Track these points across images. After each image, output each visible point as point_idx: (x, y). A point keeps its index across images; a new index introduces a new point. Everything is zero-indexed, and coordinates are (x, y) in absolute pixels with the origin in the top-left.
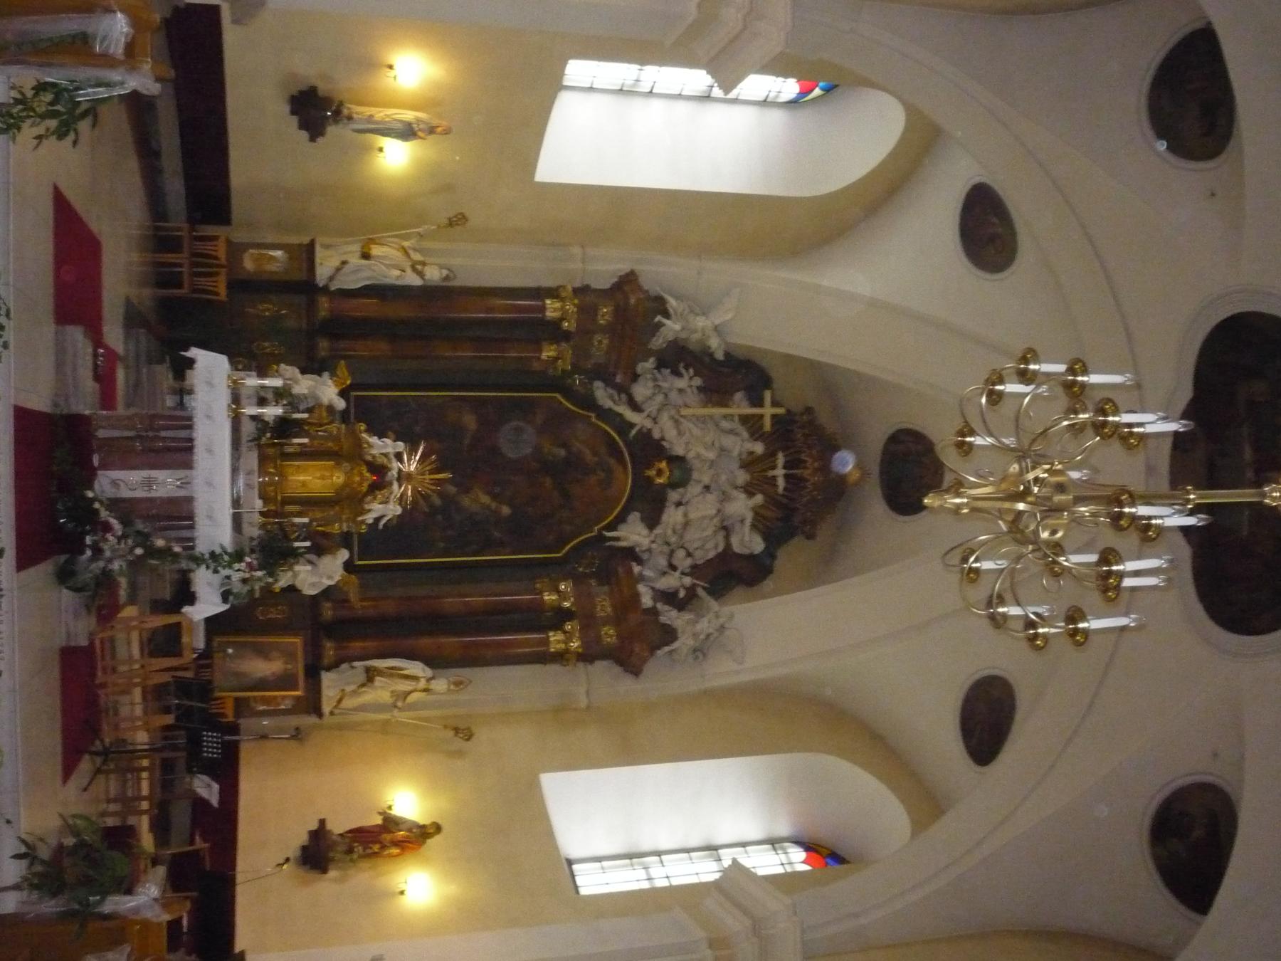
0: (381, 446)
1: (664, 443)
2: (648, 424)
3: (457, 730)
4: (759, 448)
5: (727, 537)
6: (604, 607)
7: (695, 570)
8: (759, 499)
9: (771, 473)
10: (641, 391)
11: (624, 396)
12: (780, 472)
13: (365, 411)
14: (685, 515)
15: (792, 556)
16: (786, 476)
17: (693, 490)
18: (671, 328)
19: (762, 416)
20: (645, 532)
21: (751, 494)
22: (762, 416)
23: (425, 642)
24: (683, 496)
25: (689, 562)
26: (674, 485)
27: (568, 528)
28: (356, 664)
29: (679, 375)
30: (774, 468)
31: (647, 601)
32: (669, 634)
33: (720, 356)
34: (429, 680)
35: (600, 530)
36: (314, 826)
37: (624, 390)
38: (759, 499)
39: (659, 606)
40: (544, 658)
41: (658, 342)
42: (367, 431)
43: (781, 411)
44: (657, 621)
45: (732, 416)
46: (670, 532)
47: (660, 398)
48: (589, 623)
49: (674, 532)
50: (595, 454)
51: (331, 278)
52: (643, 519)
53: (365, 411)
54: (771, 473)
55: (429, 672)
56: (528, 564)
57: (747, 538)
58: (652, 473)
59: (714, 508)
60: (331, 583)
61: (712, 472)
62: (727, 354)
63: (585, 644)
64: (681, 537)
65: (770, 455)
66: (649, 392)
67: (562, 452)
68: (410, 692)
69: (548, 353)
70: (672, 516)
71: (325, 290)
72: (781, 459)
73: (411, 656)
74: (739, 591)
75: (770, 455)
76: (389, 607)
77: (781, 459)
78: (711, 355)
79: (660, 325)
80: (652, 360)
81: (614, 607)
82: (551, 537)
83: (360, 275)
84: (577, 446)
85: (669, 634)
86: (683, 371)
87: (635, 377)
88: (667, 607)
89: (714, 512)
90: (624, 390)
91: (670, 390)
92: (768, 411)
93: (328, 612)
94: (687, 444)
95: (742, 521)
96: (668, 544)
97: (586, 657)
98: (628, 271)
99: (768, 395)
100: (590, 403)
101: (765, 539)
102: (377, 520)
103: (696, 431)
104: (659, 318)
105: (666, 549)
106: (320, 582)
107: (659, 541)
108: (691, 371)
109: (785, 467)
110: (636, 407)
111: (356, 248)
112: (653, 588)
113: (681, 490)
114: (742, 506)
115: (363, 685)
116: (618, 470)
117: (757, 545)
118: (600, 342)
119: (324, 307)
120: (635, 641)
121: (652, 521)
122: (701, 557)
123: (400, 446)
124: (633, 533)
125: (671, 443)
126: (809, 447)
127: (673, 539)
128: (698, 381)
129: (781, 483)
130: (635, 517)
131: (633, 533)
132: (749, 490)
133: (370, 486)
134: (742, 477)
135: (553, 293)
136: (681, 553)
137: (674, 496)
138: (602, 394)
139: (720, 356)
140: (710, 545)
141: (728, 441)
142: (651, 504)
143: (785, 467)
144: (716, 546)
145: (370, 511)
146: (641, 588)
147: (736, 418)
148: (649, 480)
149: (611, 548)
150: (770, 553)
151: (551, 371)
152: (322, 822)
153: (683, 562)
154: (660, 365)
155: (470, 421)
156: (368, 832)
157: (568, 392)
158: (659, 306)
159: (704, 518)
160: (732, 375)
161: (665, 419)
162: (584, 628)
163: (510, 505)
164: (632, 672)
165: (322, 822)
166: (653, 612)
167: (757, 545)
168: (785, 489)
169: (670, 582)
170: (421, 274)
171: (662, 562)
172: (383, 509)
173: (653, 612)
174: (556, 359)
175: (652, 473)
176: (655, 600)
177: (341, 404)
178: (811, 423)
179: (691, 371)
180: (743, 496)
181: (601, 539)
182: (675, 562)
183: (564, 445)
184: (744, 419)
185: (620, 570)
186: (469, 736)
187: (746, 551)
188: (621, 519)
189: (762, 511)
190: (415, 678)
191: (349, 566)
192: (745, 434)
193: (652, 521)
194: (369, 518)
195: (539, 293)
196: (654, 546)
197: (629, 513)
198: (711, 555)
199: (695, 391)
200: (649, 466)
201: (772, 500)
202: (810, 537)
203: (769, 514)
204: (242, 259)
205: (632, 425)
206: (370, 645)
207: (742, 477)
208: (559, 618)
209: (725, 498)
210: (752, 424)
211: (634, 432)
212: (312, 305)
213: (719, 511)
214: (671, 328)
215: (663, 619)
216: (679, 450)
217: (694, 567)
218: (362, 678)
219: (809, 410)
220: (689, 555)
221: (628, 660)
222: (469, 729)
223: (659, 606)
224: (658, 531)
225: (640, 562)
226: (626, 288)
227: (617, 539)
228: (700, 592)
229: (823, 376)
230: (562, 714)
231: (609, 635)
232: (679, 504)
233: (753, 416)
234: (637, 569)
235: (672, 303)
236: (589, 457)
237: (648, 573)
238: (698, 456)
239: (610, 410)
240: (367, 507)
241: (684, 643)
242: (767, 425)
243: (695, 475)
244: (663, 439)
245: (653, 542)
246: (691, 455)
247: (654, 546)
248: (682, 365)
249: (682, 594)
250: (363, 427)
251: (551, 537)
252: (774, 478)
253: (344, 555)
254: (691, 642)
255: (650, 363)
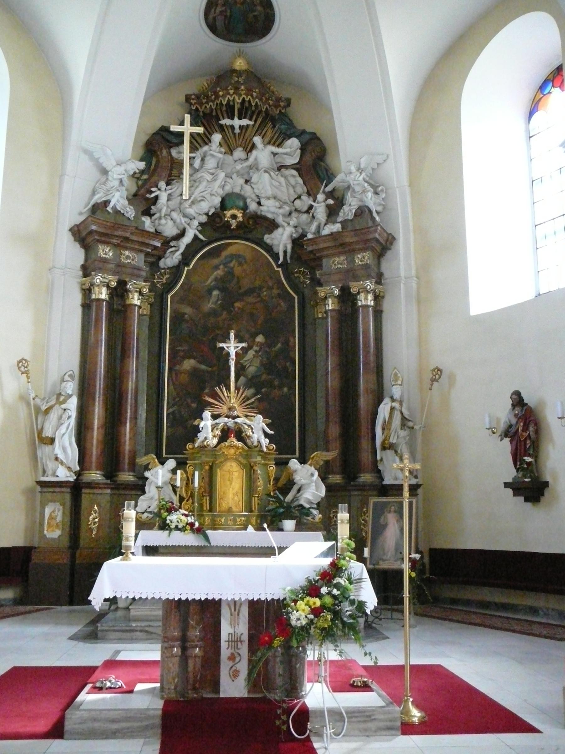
0: (208, 428)
1: (210, 214)
2: (196, 223)
3: (433, 380)
4: (217, 137)
5: (286, 167)
6: (338, 262)
7: (312, 194)
8: (257, 140)
9: (237, 131)
10: (169, 229)
11: (172, 244)
12: (237, 123)
13: (177, 442)
14: (268, 198)
15: (304, 119)
16: (240, 118)
17: (248, 191)
18: (119, 200)
19: (191, 135)
20: (280, 230)
21: (254, 146)
22: (191, 135)
23: (363, 402)
24: (253, 200)
25: (305, 197)
26: (245, 208)
27: (275, 291)
28: (379, 458)
29: (157, 198)
30: (232, 127)
31: (336, 227)
32: (363, 212)
33: (142, 165)
34: (393, 400)
35: (278, 266)
36: (510, 491)
37: (167, 243)
38: (257, 140)
39: (340, 219)
40: (378, 313)
41: (130, 212)
42: (193, 441)
43: (187, 117)
44: (351, 220)
45: (190, 158)
46: (281, 211)
47: (175, 215)
48: (352, 274)
49: (280, 208)
50: (217, 268)
51: (69, 468)
52: (271, 232)
53: (177, 442)
54: (237, 131)
55: (387, 400)
56: (302, 325)
57: (288, 150)
58: (234, 224)
59: (266, 177)
60: (316, 473)
61: (234, 176)
62: (141, 160)
63: (369, 277)
64: (285, 203)
65: (222, 129)
66: (170, 223)
67: (215, 293)
68: (402, 413)
69: (135, 299)
70: (269, 208)
71: (79, 474)
72: (226, 122)
73: (374, 414)
74: (330, 160)
75: (222, 129)
76: (335, 431)
77: (226, 122)
78: (142, 172)
79: (114, 208)
80: (143, 219)
81: (340, 254)
82: (282, 304)
83: (67, 444)
84: (210, 281)
85: (363, 212)
86: (153, 195)
87: (157, 234)
88: (341, 214)
89: (266, 175)
90: (167, 243)
91: (168, 207)
92: (188, 129)
93: (336, 479)
94: (212, 195)
95: (275, 154)
96: (290, 214)
97: (379, 279)
98: (70, 234)
99: (175, 128)
100: (176, 271)
101: (290, 137)
102: (266, 435)
103: (201, 188)
104: (109, 209)
105: (294, 215)
106: (315, 482)
107: (287, 220)
108: (153, 189)
109: (233, 119)
110: (182, 234)
111: (47, 449)
112: (325, 224)
113: (248, 201)
114: (263, 154)
115: (396, 452)
116: (230, 250)
117: (293, 143)
118: (128, 257)
119: (95, 476)
120: (368, 238)
121: (272, 225)
122: (301, 188)
123: (207, 414)
124: (281, 239)
125: (211, 207)
126: (217, 97)
127: (287, 209)
128: (162, 184)
129: (245, 122)
130: (267, 238)
131: (281, 239)
132: (250, 148)
133: (238, 441)
134: (239, 153)
135: (87, 292)
136: (298, 203)
137: (253, 206)
138: (172, 259)
139: (142, 165)
140: (292, 181)
141: (211, 163)
142: (257, 226)
143: (233, 119)
144: (293, 176)
145: (259, 442)
146: (326, 231)
147: (193, 155)
148: (240, 226)
149: (291, 258)
150: (300, 134)
151: (152, 300)
152: (507, 485)
153: (307, 201)
154: (148, 213)
155: (188, 364)
156: (516, 449)
157: (169, 286)
158: (99, 208)
159: (271, 184)
160: (158, 151)
161: (191, 211)
162: (356, 278)
163: (257, 334)
164: (391, 243)
165: (507, 485)
166: (344, 223)
167: (293, 143)
168: (250, 120)
169: (320, 211)
170: (70, 396)
171: (304, 217)
172: (257, 428)
173: (344, 223)
174: (140, 293)
175: (234, 224)
176: (334, 222)
177: (171, 463)
178: (198, 97)
179: (153, 189)
180: (254, 153)
181: (284, 265)
182: (305, 209)
183: (210, 291)
184: (193, 148)
185: (310, 249)
186: (438, 371)
187: (299, 152)
188: (269, 249)
189: (267, 139)
190: (392, 409)
191: (303, 460)
192: (206, 148)
193: (272, 225)
194: (265, 442)
195: (88, 305)
196: (292, 223)
197: (265, 243)
198: (300, 180)
199: (169, 187)
200: (228, 225)
201: (259, 131)
202: (288, 102)
203: (269, 134)
204: (53, 539)
205: (196, 238)
206: (365, 444)
207: (239, 153)
208: (347, 298)
209: (255, 167)
210: (198, 142)
211: (201, 237)
212: (91, 485)
213: (266, 171)
214: (119, 200)
215: (351, 217)
216: (217, 201)
217: (309, 194)
218: (390, 453)
219: (188, 98)
220: (299, 197)
221: (383, 246)
222: (433, 370)
223: (340, 219)
224: (280, 220)
225: (303, 235)
226: (84, 234)
227: (285, 252)
228: (329, 188)
229: (159, 89)
230: (423, 300)
231: (363, 258)
232: (259, 203)
233: (191, 142)
234: (310, 236)
235: (99, 198)
236: (219, 273)
237: (313, 227)
238: (223, 187)
239: (183, 254)
240: (256, 444)
241: (370, 200)
242: (200, 130)
243: (237, 190)
244: (207, 214)
245: (289, 224)
246: (221, 192)
247: (292, 223)
248: (148, 196)
249: (331, 202)
250: (189, 446)
251: (282, 304)
252: (241, 127)
253: (294, 464)
254: (370, 195)
255: (147, 222)
